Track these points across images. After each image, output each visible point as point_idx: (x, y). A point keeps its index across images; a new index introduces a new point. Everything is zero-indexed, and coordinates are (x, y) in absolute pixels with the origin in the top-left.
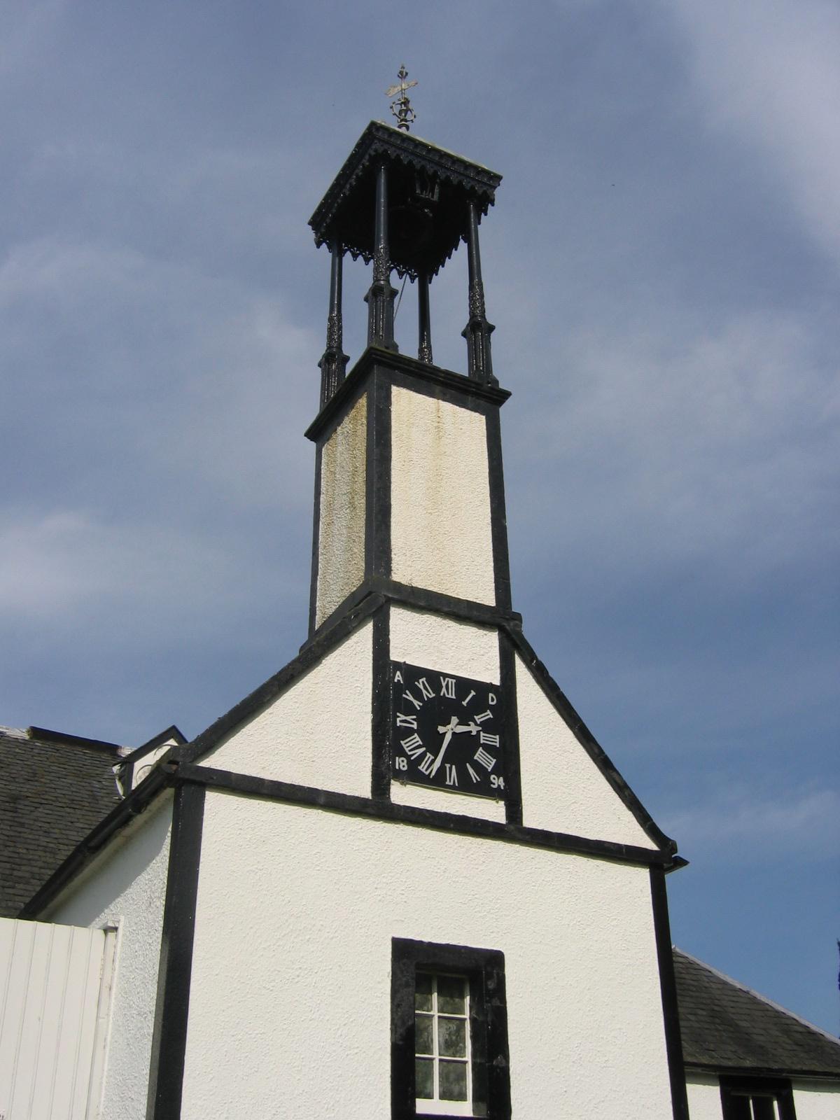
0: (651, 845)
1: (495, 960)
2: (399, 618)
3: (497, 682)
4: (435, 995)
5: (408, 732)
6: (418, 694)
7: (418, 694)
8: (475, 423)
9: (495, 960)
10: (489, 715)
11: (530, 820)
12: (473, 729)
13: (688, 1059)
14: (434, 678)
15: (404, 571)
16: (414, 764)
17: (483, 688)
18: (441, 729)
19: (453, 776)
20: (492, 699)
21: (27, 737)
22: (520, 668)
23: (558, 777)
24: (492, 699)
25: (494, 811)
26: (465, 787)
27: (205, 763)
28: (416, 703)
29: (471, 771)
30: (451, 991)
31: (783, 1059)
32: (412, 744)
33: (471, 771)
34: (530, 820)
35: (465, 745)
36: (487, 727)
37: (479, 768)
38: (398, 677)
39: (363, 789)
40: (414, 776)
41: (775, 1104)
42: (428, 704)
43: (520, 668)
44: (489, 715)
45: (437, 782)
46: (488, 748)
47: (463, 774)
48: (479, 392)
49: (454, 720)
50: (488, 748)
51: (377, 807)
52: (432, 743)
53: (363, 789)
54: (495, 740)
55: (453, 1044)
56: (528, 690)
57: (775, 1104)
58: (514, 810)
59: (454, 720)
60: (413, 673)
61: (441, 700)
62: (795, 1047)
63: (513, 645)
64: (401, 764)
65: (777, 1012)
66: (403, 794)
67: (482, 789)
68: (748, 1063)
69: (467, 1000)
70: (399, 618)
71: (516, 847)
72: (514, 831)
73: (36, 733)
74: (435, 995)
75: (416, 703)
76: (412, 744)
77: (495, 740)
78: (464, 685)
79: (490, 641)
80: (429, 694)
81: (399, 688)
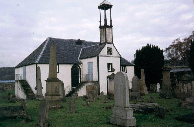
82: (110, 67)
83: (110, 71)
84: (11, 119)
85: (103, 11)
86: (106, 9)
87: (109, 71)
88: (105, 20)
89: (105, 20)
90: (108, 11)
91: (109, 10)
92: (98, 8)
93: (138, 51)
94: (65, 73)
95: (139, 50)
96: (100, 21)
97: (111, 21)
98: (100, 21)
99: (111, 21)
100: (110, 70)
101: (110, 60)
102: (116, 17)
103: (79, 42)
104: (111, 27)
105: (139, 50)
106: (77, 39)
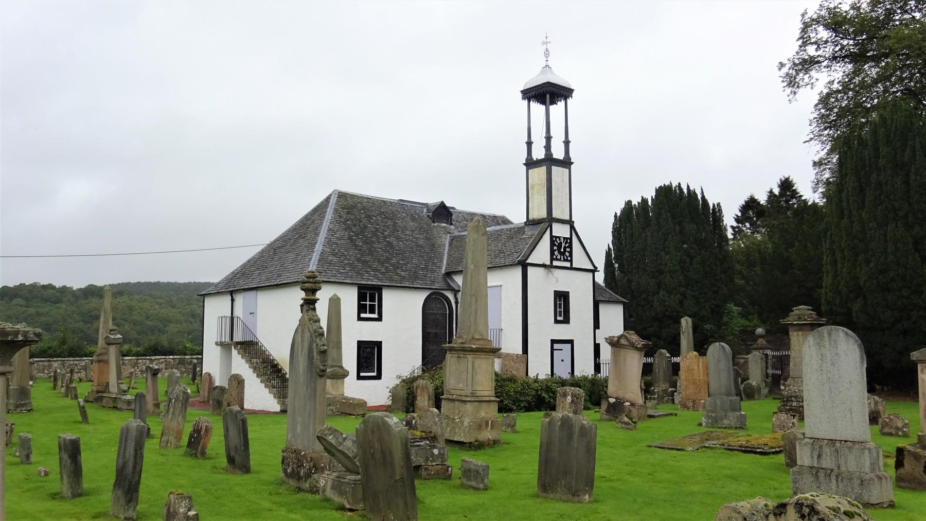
17: (567, 238)
25: (568, 264)
40: (557, 259)
45: (560, 260)
58: (571, 264)
60: (556, 237)
66: (555, 263)
67: (565, 260)
72: (571, 268)
79: (568, 227)
82: (560, 305)
83: (561, 318)
84: (748, 225)
85: (538, 109)
86: (553, 102)
87: (559, 318)
88: (548, 138)
89: (548, 138)
90: (557, 109)
91: (563, 102)
92: (520, 95)
93: (64, 287)
94: (401, 322)
95: (636, 201)
96: (529, 144)
97: (567, 143)
98: (529, 144)
99: (567, 143)
100: (560, 316)
101: (564, 280)
102: (581, 122)
103: (442, 212)
104: (566, 163)
105: (644, 201)
106: (433, 199)
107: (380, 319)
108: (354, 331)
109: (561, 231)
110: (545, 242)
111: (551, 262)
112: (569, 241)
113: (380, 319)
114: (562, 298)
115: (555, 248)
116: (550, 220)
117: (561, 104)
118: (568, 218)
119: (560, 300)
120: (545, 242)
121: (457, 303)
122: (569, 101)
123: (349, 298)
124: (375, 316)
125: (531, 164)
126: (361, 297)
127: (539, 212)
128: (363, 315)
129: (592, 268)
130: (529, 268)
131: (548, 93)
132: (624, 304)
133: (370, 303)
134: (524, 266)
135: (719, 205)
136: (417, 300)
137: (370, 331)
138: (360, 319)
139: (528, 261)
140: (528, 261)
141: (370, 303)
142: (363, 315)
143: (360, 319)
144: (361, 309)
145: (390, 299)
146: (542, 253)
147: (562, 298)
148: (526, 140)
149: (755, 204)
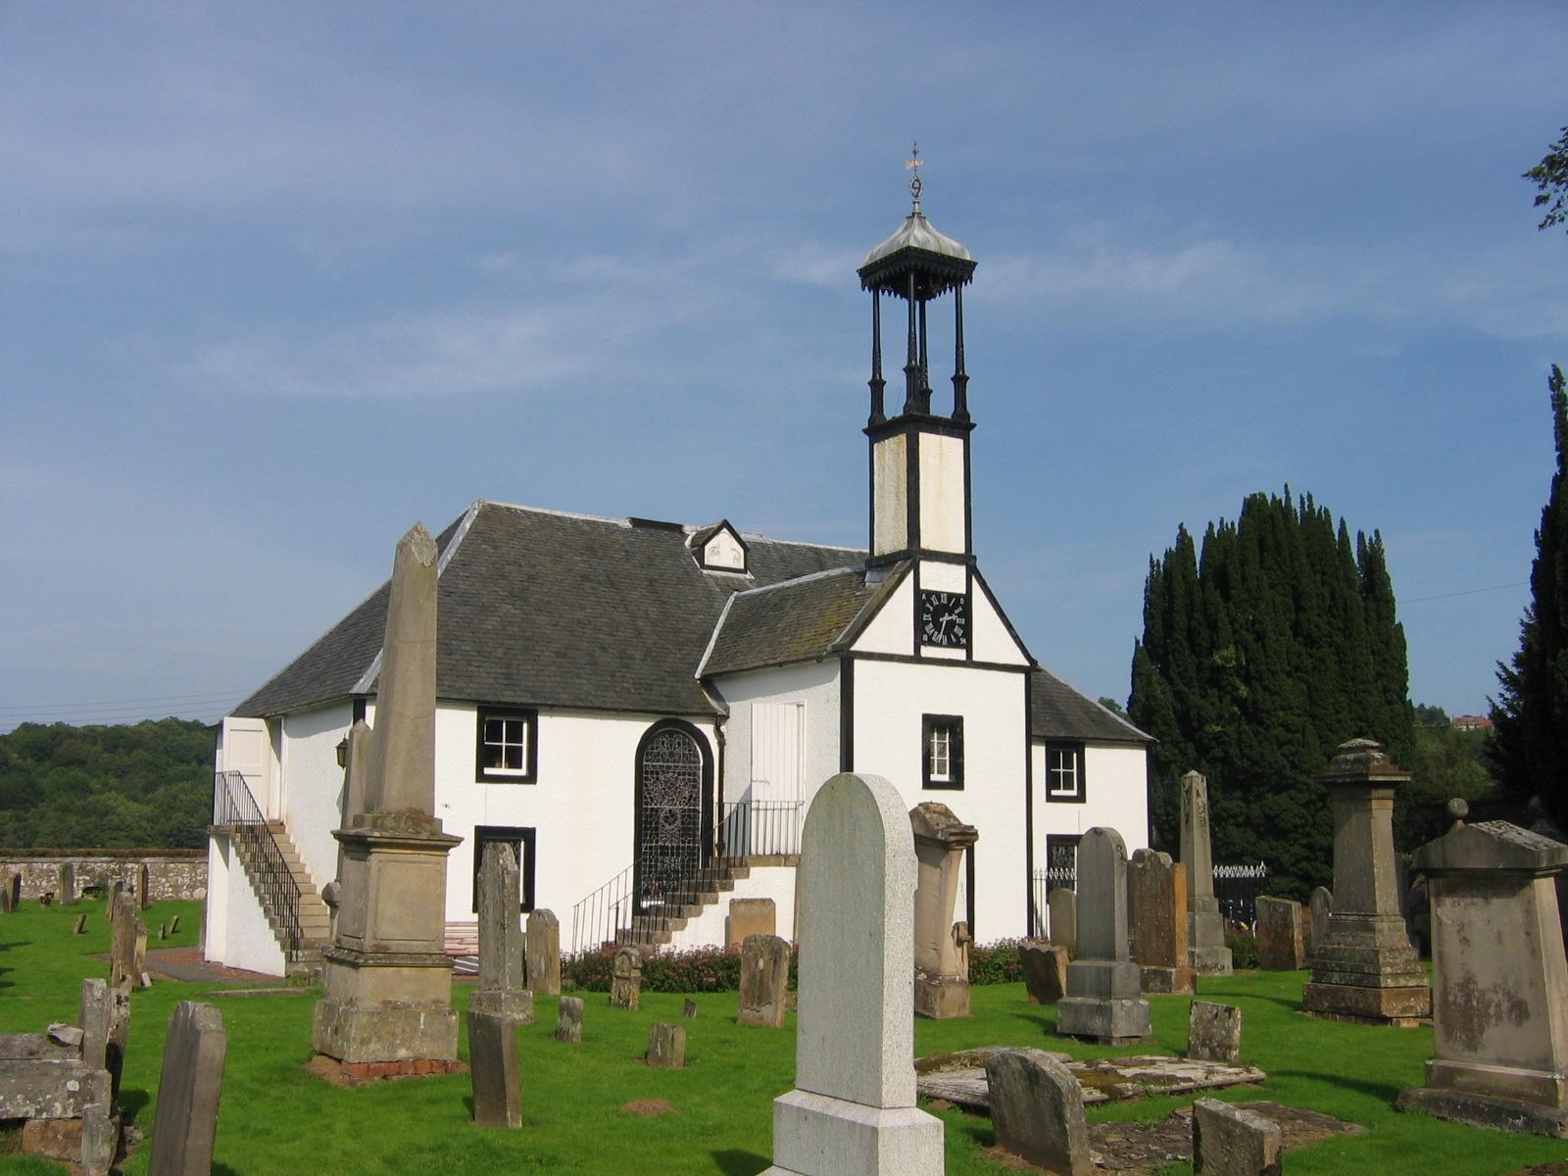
0: (1026, 663)
1: (960, 719)
2: (924, 565)
3: (964, 592)
4: (936, 734)
5: (928, 622)
6: (932, 604)
7: (932, 604)
8: (959, 443)
9: (960, 719)
10: (960, 609)
11: (976, 658)
12: (954, 617)
13: (1033, 733)
14: (938, 594)
15: (926, 543)
16: (930, 638)
17: (958, 596)
18: (941, 620)
19: (945, 642)
20: (962, 601)
21: (631, 526)
22: (975, 582)
23: (989, 636)
24: (962, 601)
25: (960, 654)
26: (951, 645)
27: (853, 649)
28: (931, 608)
29: (953, 637)
30: (941, 732)
31: (1083, 731)
32: (929, 629)
33: (953, 637)
34: (976, 658)
35: (951, 624)
36: (960, 615)
37: (956, 636)
38: (924, 596)
39: (911, 652)
40: (931, 643)
41: (1075, 755)
42: (936, 608)
43: (975, 582)
44: (960, 609)
45: (939, 645)
46: (960, 625)
47: (949, 639)
48: (959, 426)
49: (947, 614)
50: (960, 625)
51: (917, 659)
52: (937, 626)
53: (911, 652)
54: (963, 621)
55: (941, 753)
56: (979, 597)
57: (1075, 755)
58: (969, 654)
59: (947, 614)
60: (929, 593)
61: (941, 604)
62: (1090, 722)
63: (972, 572)
64: (925, 638)
65: (1083, 698)
66: (927, 652)
67: (958, 645)
68: (1062, 734)
69: (948, 735)
70: (924, 565)
71: (969, 670)
72: (969, 663)
73: (636, 522)
74: (936, 734)
75: (931, 608)
76: (929, 629)
77: (963, 621)
78: (950, 596)
79: (961, 571)
80: (936, 603)
81: (924, 602)
85: (895, 307)
87: (935, 777)
90: (940, 306)
94: (585, 780)
96: (877, 385)
97: (960, 381)
98: (877, 385)
99: (960, 381)
100: (941, 772)
107: (531, 778)
108: (463, 801)
109: (945, 579)
110: (902, 603)
111: (917, 649)
112: (961, 605)
113: (531, 778)
114: (944, 731)
115: (927, 617)
116: (913, 555)
117: (948, 297)
118: (961, 549)
119: (941, 737)
120: (902, 603)
121: (722, 745)
122: (965, 289)
123: (456, 731)
124: (1074, 793)
125: (878, 430)
126: (487, 731)
127: (891, 538)
128: (1054, 793)
129: (1026, 663)
130: (858, 664)
131: (915, 276)
132: (1149, 747)
133: (504, 746)
134: (846, 661)
135: (1326, 511)
136: (619, 739)
137: (505, 805)
138: (481, 778)
139: (857, 647)
140: (857, 647)
141: (504, 746)
142: (1054, 793)
143: (481, 778)
144: (486, 756)
145: (555, 733)
146: (893, 624)
147: (944, 731)
148: (870, 378)
149: (615, 528)
